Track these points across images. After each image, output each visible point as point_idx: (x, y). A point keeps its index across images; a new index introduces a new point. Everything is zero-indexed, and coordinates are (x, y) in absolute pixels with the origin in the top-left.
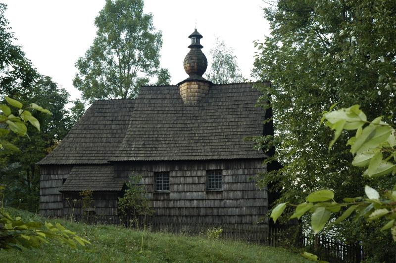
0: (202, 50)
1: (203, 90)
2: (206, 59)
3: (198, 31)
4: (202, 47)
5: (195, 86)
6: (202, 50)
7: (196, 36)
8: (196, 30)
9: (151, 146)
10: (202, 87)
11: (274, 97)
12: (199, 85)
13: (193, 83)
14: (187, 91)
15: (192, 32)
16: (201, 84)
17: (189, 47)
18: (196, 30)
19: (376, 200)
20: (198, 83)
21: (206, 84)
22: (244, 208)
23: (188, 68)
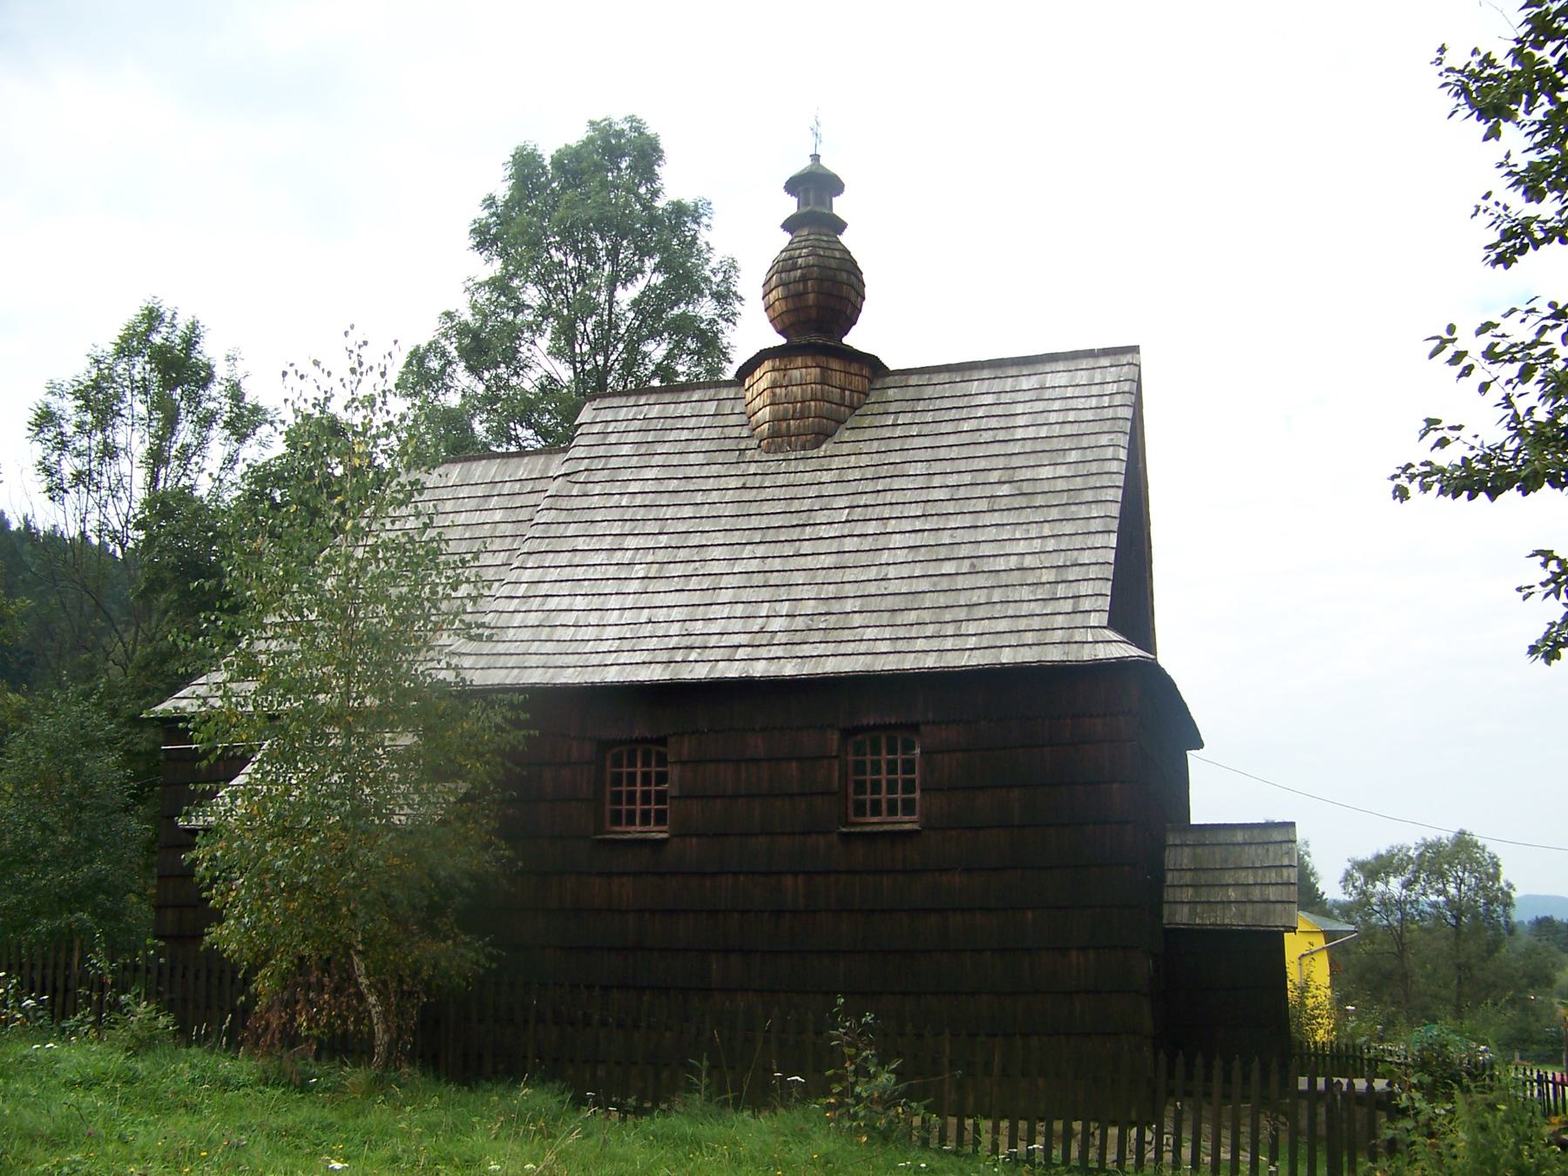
0: (845, 239)
1: (843, 389)
2: (854, 263)
3: (823, 162)
5: (804, 373)
7: (1432, 356)
8: (816, 157)
9: (507, 543)
10: (837, 378)
11: (675, 241)
12: (824, 369)
13: (799, 361)
14: (774, 394)
15: (801, 164)
16: (835, 364)
18: (816, 157)
19: (38, 532)
20: (822, 360)
21: (854, 368)
22: (1074, 954)
23: (779, 307)
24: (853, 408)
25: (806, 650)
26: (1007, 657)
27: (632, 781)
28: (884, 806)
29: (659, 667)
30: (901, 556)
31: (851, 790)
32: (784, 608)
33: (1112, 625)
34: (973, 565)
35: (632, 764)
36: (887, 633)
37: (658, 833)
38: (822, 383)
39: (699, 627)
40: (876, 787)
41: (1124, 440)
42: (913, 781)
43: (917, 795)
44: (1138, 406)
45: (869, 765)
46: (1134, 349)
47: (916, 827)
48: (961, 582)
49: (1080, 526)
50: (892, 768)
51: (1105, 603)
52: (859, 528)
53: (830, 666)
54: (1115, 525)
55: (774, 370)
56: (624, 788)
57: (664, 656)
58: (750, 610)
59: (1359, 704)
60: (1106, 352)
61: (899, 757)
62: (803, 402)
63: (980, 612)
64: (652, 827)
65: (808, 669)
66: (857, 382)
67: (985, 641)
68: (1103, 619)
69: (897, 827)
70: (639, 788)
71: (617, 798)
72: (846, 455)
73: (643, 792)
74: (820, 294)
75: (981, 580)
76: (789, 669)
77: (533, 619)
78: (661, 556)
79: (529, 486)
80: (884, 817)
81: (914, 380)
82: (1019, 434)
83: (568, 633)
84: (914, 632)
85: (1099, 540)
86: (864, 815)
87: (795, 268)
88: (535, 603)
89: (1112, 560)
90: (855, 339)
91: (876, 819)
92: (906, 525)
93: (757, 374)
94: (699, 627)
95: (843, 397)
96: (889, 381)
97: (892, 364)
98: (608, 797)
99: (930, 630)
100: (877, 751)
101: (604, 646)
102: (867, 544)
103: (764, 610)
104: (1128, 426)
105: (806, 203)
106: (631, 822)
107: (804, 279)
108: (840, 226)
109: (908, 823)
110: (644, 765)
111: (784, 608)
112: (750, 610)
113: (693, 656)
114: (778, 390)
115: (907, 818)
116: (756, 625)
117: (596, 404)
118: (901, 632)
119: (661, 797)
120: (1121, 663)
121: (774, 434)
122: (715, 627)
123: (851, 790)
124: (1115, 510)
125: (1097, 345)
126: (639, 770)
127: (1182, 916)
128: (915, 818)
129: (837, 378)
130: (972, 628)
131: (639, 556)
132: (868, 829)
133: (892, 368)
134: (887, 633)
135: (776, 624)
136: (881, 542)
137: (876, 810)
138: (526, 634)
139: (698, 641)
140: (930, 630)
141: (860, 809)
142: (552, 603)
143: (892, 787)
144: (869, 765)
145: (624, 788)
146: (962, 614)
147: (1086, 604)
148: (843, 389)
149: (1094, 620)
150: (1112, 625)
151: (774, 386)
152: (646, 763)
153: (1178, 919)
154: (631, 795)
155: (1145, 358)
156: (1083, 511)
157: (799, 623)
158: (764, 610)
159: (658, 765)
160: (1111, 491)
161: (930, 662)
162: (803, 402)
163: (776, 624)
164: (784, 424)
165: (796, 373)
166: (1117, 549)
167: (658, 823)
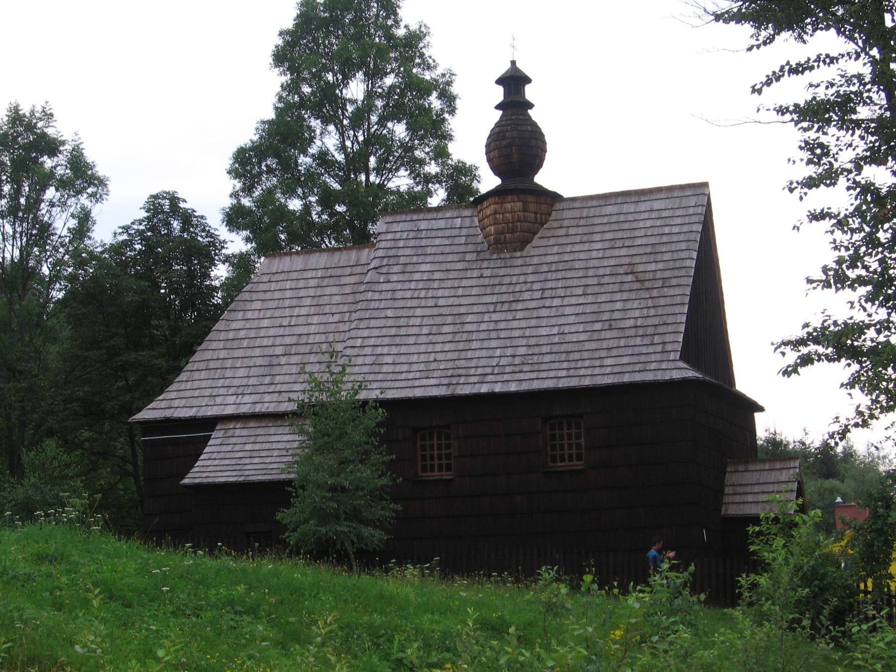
1: (536, 213)
3: (518, 65)
4: (531, 106)
8: (513, 63)
10: (532, 207)
12: (525, 203)
13: (510, 198)
15: (503, 68)
16: (531, 198)
17: (498, 107)
18: (513, 63)
24: (542, 224)
25: (522, 376)
26: (626, 379)
27: (432, 449)
28: (566, 457)
29: (444, 388)
30: (572, 319)
31: (549, 449)
32: (509, 352)
33: (683, 358)
34: (610, 325)
35: (431, 439)
36: (565, 365)
37: (446, 475)
38: (524, 211)
39: (462, 363)
40: (562, 448)
43: (583, 451)
45: (566, 446)
46: (706, 185)
48: (604, 335)
49: (669, 301)
50: (570, 436)
52: (548, 303)
53: (536, 385)
54: (687, 300)
55: (495, 203)
56: (444, 462)
57: (446, 381)
58: (490, 353)
61: (574, 431)
62: (513, 223)
63: (614, 352)
64: (444, 473)
65: (525, 387)
66: (544, 208)
67: (616, 369)
69: (575, 468)
71: (424, 458)
72: (543, 250)
73: (438, 454)
74: (518, 142)
75: (614, 334)
76: (513, 387)
77: (369, 360)
78: (438, 320)
79: (348, 271)
80: (567, 463)
81: (577, 205)
82: (639, 242)
83: (390, 368)
84: (580, 364)
85: (677, 310)
86: (556, 462)
87: (504, 138)
88: (368, 351)
91: (563, 464)
92: (574, 301)
93: (485, 204)
94: (462, 363)
95: (536, 218)
98: (419, 458)
99: (587, 363)
100: (561, 429)
101: (411, 376)
102: (553, 312)
103: (498, 353)
106: (432, 470)
107: (510, 145)
109: (578, 465)
111: (509, 352)
112: (490, 353)
113: (462, 380)
114: (498, 216)
115: (578, 463)
116: (494, 362)
117: (389, 219)
118: (573, 365)
119: (448, 457)
120: (684, 382)
121: (497, 242)
122: (473, 363)
124: (688, 291)
127: (732, 511)
128: (582, 462)
130: (609, 362)
131: (426, 321)
132: (559, 469)
133: (565, 196)
134: (565, 365)
135: (503, 361)
136: (561, 311)
137: (562, 459)
138: (365, 369)
139: (463, 372)
140: (587, 363)
141: (554, 459)
142: (379, 350)
143: (570, 447)
144: (566, 446)
145: (444, 462)
146: (604, 354)
147: (669, 347)
149: (672, 356)
150: (683, 358)
151: (496, 212)
152: (439, 439)
153: (729, 512)
156: (672, 292)
157: (517, 361)
158: (498, 353)
160: (686, 279)
161: (587, 382)
162: (513, 223)
163: (503, 361)
164: (502, 237)
165: (508, 206)
167: (447, 471)
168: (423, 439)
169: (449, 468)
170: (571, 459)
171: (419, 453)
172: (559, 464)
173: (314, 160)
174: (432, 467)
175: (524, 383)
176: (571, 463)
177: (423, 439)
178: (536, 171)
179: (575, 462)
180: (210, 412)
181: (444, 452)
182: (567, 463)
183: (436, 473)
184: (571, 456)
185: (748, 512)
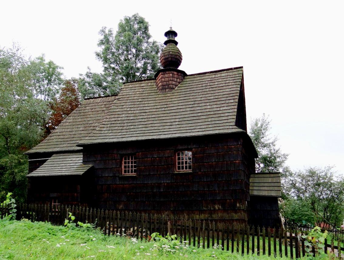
1: (177, 79)
6: (178, 46)
8: (171, 28)
12: (173, 74)
13: (167, 72)
27: (129, 163)
31: (177, 164)
35: (129, 159)
41: (239, 86)
42: (178, 160)
44: (243, 79)
46: (242, 67)
47: (191, 172)
51: (234, 120)
55: (162, 75)
56: (127, 165)
59: (303, 139)
60: (235, 68)
62: (168, 81)
64: (188, 170)
68: (234, 124)
70: (130, 165)
71: (125, 167)
74: (172, 61)
80: (127, 174)
89: (239, 95)
90: (180, 68)
95: (177, 80)
96: (188, 77)
97: (188, 73)
104: (240, 83)
105: (169, 38)
106: (129, 172)
108: (176, 43)
110: (131, 160)
114: (163, 79)
123: (177, 164)
125: (233, 67)
126: (184, 165)
128: (191, 170)
129: (176, 76)
132: (181, 172)
133: (188, 74)
141: (179, 168)
148: (177, 79)
150: (236, 125)
152: (132, 159)
154: (129, 166)
155: (244, 69)
159: (128, 160)
166: (237, 112)
168: (125, 159)
169: (190, 167)
170: (186, 168)
171: (123, 165)
172: (181, 170)
173: (333, 205)
174: (183, 167)
175: (125, 129)
176: (129, 174)
177: (125, 159)
178: (178, 67)
179: (133, 173)
180: (51, 150)
181: (127, 165)
182: (188, 170)
183: (130, 173)
184: (186, 167)
185: (261, 194)
